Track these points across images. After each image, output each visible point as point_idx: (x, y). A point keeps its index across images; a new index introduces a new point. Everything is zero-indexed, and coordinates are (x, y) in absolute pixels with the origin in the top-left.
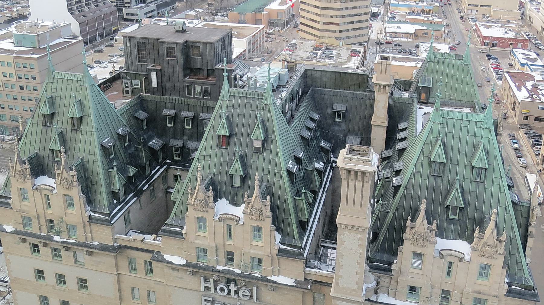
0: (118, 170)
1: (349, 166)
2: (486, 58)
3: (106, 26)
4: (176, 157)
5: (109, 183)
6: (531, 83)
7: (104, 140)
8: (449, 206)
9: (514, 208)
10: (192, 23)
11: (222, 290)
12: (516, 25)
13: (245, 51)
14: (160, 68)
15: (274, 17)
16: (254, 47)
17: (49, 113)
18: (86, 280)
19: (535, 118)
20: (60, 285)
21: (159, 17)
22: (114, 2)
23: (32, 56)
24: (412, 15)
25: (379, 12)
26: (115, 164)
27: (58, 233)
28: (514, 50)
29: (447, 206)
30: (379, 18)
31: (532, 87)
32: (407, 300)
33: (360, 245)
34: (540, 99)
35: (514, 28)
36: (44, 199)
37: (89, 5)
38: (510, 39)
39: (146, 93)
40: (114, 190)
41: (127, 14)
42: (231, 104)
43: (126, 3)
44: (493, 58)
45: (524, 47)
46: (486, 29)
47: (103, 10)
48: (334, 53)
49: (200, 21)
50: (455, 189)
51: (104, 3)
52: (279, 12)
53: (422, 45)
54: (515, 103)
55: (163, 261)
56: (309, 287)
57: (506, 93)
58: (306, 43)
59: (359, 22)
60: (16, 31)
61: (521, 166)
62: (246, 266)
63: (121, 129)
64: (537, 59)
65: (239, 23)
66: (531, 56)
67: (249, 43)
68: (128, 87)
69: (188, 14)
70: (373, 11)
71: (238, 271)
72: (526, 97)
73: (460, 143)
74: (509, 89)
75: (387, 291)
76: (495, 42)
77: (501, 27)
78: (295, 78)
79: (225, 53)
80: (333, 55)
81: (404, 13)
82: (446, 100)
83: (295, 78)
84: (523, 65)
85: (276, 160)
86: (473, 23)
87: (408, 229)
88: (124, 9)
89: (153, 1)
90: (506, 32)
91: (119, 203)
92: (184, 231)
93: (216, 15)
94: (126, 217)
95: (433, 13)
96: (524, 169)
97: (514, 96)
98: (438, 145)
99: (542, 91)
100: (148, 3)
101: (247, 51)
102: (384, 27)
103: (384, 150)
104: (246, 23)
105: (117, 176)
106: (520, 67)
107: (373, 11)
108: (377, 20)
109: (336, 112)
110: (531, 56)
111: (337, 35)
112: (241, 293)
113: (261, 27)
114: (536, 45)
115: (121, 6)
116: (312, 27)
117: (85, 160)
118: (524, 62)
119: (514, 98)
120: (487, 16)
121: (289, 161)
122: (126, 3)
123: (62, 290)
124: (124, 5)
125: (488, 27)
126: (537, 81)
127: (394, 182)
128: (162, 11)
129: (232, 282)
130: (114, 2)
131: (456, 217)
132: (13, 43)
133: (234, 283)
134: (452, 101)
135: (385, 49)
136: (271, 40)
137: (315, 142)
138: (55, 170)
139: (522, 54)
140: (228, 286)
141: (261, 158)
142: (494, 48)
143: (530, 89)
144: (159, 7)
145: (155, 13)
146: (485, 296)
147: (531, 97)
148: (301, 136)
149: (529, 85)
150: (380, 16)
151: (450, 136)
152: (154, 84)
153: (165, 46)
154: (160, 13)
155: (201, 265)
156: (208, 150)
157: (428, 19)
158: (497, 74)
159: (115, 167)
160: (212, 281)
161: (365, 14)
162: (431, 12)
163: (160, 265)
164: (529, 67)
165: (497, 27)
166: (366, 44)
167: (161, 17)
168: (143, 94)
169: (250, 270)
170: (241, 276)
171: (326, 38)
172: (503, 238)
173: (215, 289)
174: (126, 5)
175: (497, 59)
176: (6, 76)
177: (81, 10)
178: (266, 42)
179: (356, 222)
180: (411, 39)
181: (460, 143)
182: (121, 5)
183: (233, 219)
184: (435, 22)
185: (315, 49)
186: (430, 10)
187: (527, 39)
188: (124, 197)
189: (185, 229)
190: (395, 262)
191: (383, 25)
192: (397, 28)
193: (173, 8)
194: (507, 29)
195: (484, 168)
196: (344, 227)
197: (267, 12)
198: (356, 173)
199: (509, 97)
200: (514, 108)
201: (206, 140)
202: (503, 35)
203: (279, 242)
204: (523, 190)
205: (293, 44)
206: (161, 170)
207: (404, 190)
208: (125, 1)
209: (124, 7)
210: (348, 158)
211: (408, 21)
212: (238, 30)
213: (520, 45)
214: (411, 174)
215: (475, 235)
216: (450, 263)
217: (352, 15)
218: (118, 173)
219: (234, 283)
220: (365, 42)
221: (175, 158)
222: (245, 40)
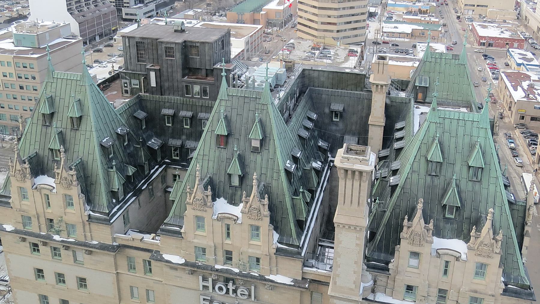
0: (117, 169)
1: (347, 165)
2: (483, 57)
3: (105, 26)
4: (175, 156)
5: (108, 183)
6: (527, 82)
7: (103, 140)
8: (446, 205)
9: (510, 207)
10: (191, 23)
11: (220, 289)
12: (513, 24)
13: (243, 51)
14: (158, 68)
15: (272, 17)
16: (252, 47)
17: (48, 113)
18: (85, 279)
19: (531, 117)
20: (59, 284)
21: (157, 17)
22: (114, 2)
23: (32, 56)
24: (409, 15)
25: (376, 12)
26: (114, 164)
27: (58, 233)
28: (510, 50)
29: (444, 205)
30: (376, 18)
31: (528, 87)
32: (404, 299)
33: (357, 245)
34: (536, 98)
35: (510, 28)
36: (43, 198)
37: (88, 5)
38: (506, 39)
39: (144, 92)
40: (113, 190)
41: (126, 14)
42: (229, 104)
43: (125, 3)
44: (489, 57)
45: (520, 47)
46: (482, 29)
47: (102, 10)
48: (332, 53)
49: (199, 21)
50: (452, 189)
51: (103, 3)
52: (277, 12)
53: (419, 45)
54: (511, 102)
55: (162, 260)
56: (307, 286)
57: (503, 93)
58: (304, 42)
59: (357, 22)
60: (16, 31)
61: (517, 166)
62: (244, 265)
63: (121, 128)
64: (534, 59)
65: (237, 23)
66: (527, 55)
67: (247, 43)
68: (127, 87)
69: (186, 14)
70: (370, 11)
71: (237, 270)
72: (522, 97)
73: (456, 143)
74: (505, 88)
75: (385, 290)
76: (491, 42)
77: (497, 27)
78: (293, 77)
79: (223, 53)
80: (331, 54)
81: (401, 13)
82: (443, 100)
83: (293, 77)
84: (519, 65)
85: (274, 159)
86: (469, 23)
87: (405, 229)
88: (123, 9)
89: (152, 1)
90: (502, 32)
91: (118, 202)
92: (182, 231)
93: (215, 15)
94: (125, 216)
95: (429, 13)
96: (520, 168)
97: (511, 96)
98: (435, 145)
99: (538, 91)
100: (146, 3)
101: (245, 51)
102: (381, 27)
103: (381, 149)
104: (244, 23)
105: (116, 176)
106: (516, 67)
107: (370, 11)
108: (375, 20)
109: (333, 111)
110: (527, 55)
111: (335, 35)
112: (239, 292)
113: (259, 27)
114: (532, 45)
115: (120, 6)
116: (310, 27)
117: (85, 159)
118: (520, 61)
119: (510, 98)
120: (483, 16)
121: (287, 161)
122: (125, 3)
123: (61, 289)
124: (123, 5)
125: (484, 27)
126: (534, 81)
127: (391, 181)
128: (161, 11)
129: (230, 281)
130: (114, 2)
131: (453, 217)
132: (13, 42)
133: (232, 282)
134: (448, 101)
135: (382, 49)
136: (269, 40)
137: (313, 142)
138: (55, 170)
139: (518, 53)
140: (227, 285)
141: (259, 157)
142: (490, 48)
143: (526, 89)
144: (158, 7)
145: (154, 13)
146: (482, 295)
147: (527, 96)
148: (299, 135)
149: (525, 84)
150: (377, 16)
151: (447, 135)
152: (153, 84)
153: (164, 46)
154: (159, 13)
155: (200, 264)
156: (207, 150)
157: (425, 19)
158: (493, 73)
159: (114, 166)
160: (210, 280)
161: (363, 14)
162: (428, 12)
163: (159, 264)
164: (525, 67)
165: (493, 26)
166: (363, 44)
167: (160, 17)
168: (142, 94)
169: (248, 269)
170: (239, 275)
171: (324, 38)
172: (500, 237)
173: (214, 288)
174: (125, 5)
175: (494, 59)
176: (6, 76)
177: (81, 10)
178: (264, 42)
179: (353, 222)
180: (408, 39)
181: (456, 143)
182: (120, 5)
183: (232, 218)
184: (431, 22)
185: (313, 48)
186: (427, 10)
187: (523, 38)
188: (123, 196)
189: (183, 228)
190: (392, 261)
191: (380, 25)
192: (394, 28)
193: (171, 8)
194: (503, 29)
195: (481, 168)
196: (341, 226)
197: (265, 12)
198: (354, 172)
199: (505, 97)
200: (510, 108)
201: (204, 140)
202: (499, 35)
203: (277, 241)
204: (519, 189)
205: (291, 43)
206: (160, 170)
207: (401, 190)
208: (124, 1)
209: (123, 7)
210: (345, 158)
211: (405, 21)
212: (237, 30)
213: (516, 45)
214: (408, 174)
215: (471, 234)
216: (447, 262)
217: (349, 15)
218: (117, 173)
219: (232, 282)
220: (362, 42)
221: (174, 158)
222: (243, 40)
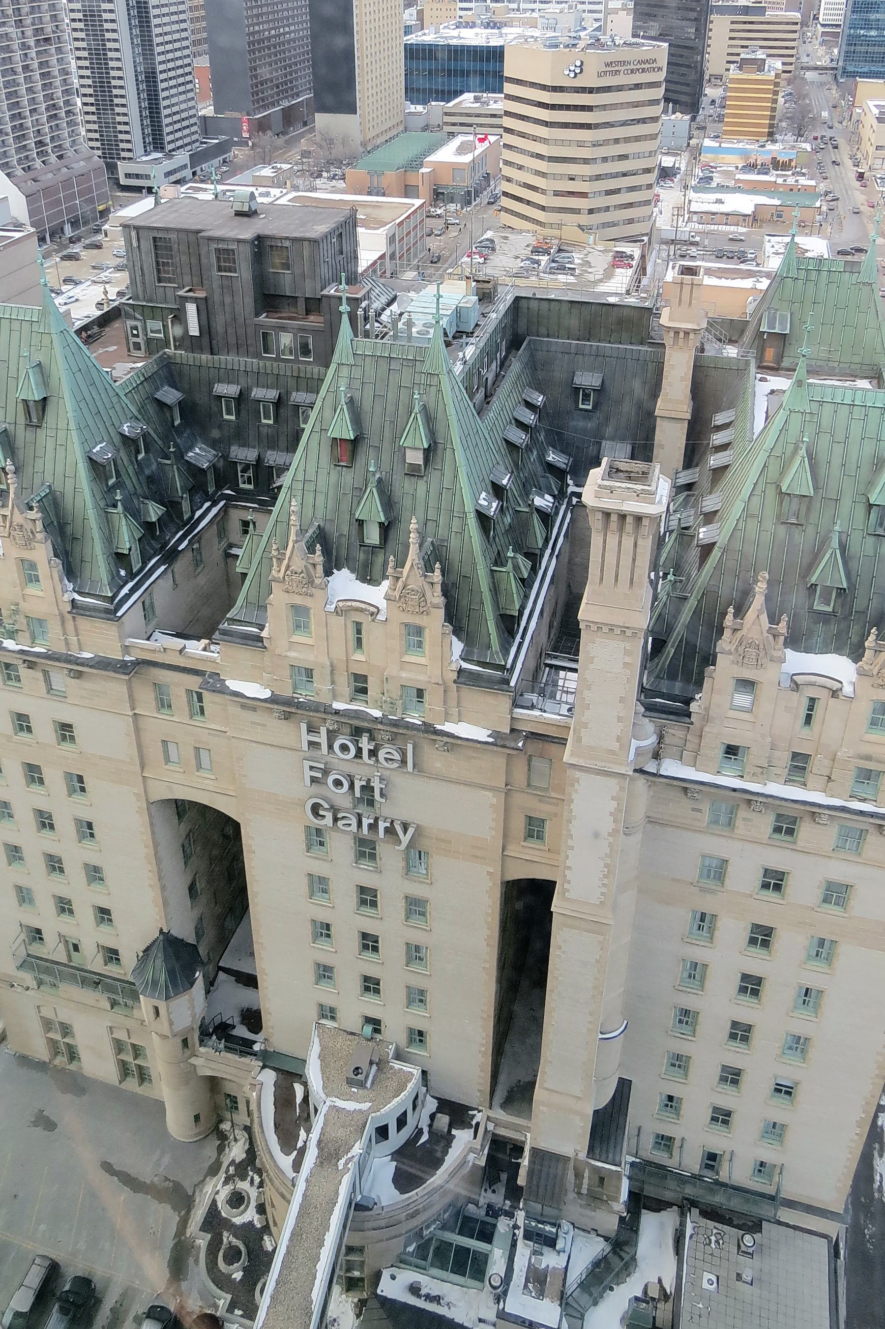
0: (126, 509)
1: (609, 503)
4: (244, 483)
5: (110, 537)
7: (94, 448)
10: (267, 194)
11: (344, 748)
13: (382, 257)
15: (446, 179)
18: (70, 726)
24: (749, 172)
32: (718, 772)
39: (175, 349)
41: (126, 174)
42: (357, 373)
48: (577, 261)
49: (285, 191)
50: (830, 552)
51: (75, 151)
55: (224, 690)
59: (632, 189)
63: (128, 424)
67: (391, 240)
68: (137, 336)
69: (258, 174)
71: (377, 713)
82: (820, 363)
85: (454, 490)
88: (119, 163)
91: (131, 575)
93: (320, 176)
94: (147, 603)
98: (798, 460)
100: (170, 151)
103: (680, 469)
104: (384, 195)
112: (382, 754)
115: (113, 158)
116: (528, 203)
127: (701, 536)
131: (830, 609)
134: (831, 364)
136: (439, 233)
140: (357, 741)
141: (421, 485)
145: (187, 173)
151: (825, 439)
154: (199, 173)
155: (301, 700)
157: (785, 181)
161: (648, 171)
162: (793, 164)
163: (218, 698)
167: (202, 181)
170: (381, 723)
173: (330, 747)
177: (29, 167)
179: (619, 619)
185: (536, 251)
190: (697, 697)
191: (685, 195)
196: (594, 627)
198: (623, 517)
201: (306, 448)
205: (487, 240)
206: (215, 511)
207: (723, 554)
209: (119, 159)
211: (739, 187)
218: (126, 516)
219: (368, 735)
220: (643, 235)
221: (242, 486)
222: (383, 231)
